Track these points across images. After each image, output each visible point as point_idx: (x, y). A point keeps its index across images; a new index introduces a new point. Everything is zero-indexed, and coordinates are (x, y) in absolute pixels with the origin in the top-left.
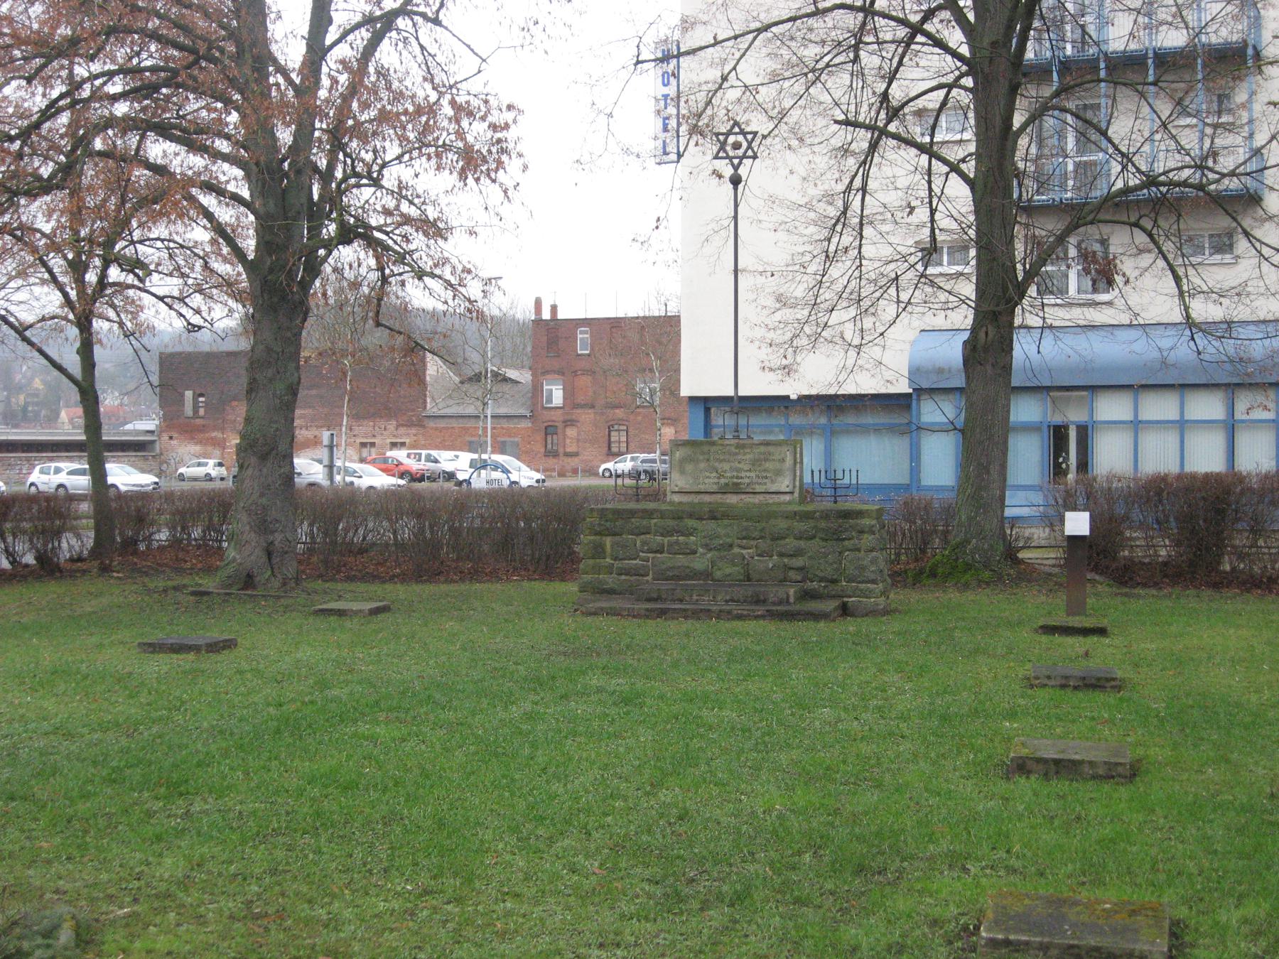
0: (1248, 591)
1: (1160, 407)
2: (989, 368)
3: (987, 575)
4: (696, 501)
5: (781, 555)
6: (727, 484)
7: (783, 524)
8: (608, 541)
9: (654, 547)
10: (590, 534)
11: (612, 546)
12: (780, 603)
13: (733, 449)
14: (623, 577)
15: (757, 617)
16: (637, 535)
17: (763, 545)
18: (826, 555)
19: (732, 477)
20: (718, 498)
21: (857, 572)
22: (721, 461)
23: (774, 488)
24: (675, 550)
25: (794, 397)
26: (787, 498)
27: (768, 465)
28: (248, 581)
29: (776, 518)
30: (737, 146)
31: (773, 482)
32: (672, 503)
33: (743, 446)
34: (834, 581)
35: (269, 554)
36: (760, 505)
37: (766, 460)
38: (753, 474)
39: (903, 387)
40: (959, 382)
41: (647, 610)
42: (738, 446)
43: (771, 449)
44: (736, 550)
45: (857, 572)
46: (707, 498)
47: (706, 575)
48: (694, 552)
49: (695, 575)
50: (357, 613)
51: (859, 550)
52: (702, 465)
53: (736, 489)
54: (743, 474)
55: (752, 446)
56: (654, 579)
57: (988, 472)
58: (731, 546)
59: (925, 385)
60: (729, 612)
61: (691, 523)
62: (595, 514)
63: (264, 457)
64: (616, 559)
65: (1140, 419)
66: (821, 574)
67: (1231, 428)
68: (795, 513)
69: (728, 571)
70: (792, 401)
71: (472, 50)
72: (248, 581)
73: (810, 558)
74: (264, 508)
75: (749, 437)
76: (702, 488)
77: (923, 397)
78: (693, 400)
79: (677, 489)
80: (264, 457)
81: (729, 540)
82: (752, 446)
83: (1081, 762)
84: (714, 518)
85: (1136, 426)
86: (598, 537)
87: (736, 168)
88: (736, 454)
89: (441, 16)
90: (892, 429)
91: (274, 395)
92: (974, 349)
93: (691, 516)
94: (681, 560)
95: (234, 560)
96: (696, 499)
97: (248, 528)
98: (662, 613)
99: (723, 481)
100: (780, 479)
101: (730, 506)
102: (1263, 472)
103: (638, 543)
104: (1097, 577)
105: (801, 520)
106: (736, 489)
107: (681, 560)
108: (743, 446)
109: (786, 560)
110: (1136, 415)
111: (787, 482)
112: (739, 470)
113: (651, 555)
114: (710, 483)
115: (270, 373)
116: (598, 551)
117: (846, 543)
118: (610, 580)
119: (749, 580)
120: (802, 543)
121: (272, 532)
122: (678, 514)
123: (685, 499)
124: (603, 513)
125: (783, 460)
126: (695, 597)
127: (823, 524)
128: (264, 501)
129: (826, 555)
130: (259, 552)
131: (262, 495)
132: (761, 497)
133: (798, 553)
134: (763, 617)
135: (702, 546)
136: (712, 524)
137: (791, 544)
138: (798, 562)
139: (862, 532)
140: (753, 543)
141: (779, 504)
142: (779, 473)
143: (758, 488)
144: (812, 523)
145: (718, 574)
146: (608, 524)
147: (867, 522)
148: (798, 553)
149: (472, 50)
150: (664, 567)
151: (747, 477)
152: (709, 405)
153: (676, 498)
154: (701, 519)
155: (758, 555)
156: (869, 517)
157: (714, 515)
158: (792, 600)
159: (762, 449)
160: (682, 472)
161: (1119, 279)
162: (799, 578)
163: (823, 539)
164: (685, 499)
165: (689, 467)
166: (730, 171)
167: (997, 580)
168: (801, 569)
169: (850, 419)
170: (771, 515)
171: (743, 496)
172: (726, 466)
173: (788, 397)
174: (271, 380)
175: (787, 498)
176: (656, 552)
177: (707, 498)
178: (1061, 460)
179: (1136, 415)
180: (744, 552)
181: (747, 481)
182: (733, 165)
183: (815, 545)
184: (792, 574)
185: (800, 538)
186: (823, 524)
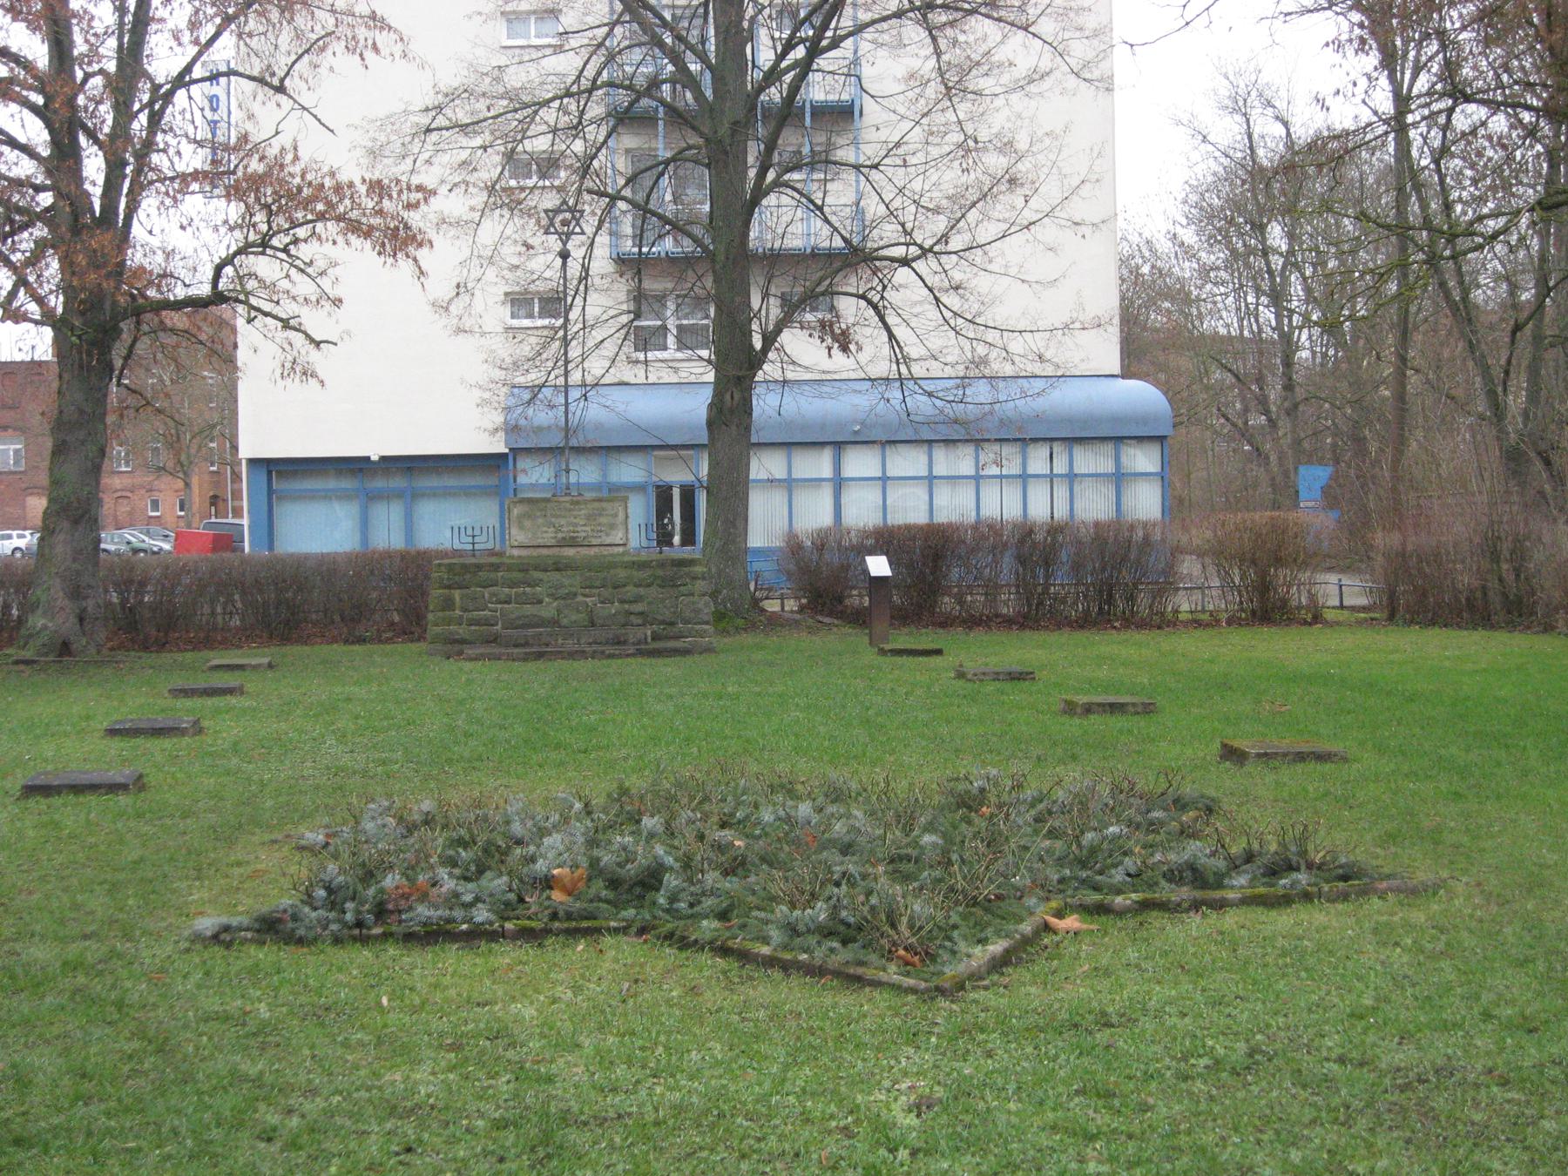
0: (970, 628)
1: (908, 462)
2: (734, 428)
3: (740, 622)
4: (535, 554)
5: (622, 602)
6: (564, 538)
7: (622, 574)
8: (457, 594)
9: (502, 597)
10: (440, 588)
11: (461, 599)
12: (639, 643)
13: (568, 505)
14: (473, 628)
15: (628, 656)
16: (484, 587)
17: (606, 593)
18: (663, 600)
19: (569, 531)
20: (555, 551)
21: (693, 615)
22: (560, 516)
23: (608, 541)
24: (522, 600)
25: (375, 458)
26: (621, 549)
27: (603, 520)
28: (65, 649)
29: (616, 567)
30: (565, 223)
31: (607, 535)
32: (512, 557)
33: (578, 503)
34: (672, 624)
35: (81, 620)
36: (596, 556)
37: (600, 515)
38: (588, 529)
39: (498, 446)
40: (704, 439)
41: (526, 653)
42: (572, 503)
43: (604, 505)
44: (580, 598)
45: (693, 615)
46: (545, 552)
47: (554, 622)
48: (540, 602)
49: (542, 623)
50: (255, 667)
51: (693, 595)
52: (540, 521)
53: (572, 542)
54: (579, 529)
55: (586, 502)
56: (503, 628)
57: (734, 526)
58: (575, 595)
59: (522, 444)
60: (603, 652)
61: (537, 575)
62: (443, 568)
63: (76, 522)
64: (465, 610)
65: (1076, 471)
66: (660, 618)
67: (839, 483)
68: (634, 563)
69: (574, 618)
70: (374, 462)
71: (319, 120)
72: (65, 649)
73: (649, 603)
74: (78, 573)
75: (580, 495)
76: (540, 542)
77: (793, 455)
78: (253, 462)
79: (516, 544)
80: (76, 522)
81: (574, 589)
82: (586, 502)
83: (1127, 704)
84: (558, 570)
85: (789, 485)
86: (447, 591)
87: (564, 244)
88: (570, 510)
89: (287, 82)
90: (485, 492)
91: (86, 457)
92: (720, 411)
93: (536, 568)
94: (529, 609)
95: (45, 627)
96: (535, 552)
97: (61, 594)
98: (540, 656)
99: (560, 535)
100: (614, 532)
101: (567, 557)
102: (871, 525)
103: (487, 595)
104: (836, 622)
105: (638, 570)
106: (572, 542)
107: (529, 609)
108: (578, 503)
109: (626, 606)
110: (1052, 469)
111: (620, 535)
112: (576, 525)
113: (499, 606)
114: (548, 536)
115: (81, 435)
116: (448, 604)
117: (682, 588)
118: (462, 631)
119: (593, 624)
120: (642, 591)
121: (85, 598)
122: (524, 567)
123: (524, 553)
124: (450, 567)
125: (616, 515)
126: (560, 641)
127: (660, 572)
128: (76, 566)
129: (663, 600)
130: (73, 620)
131: (74, 560)
132: (596, 550)
133: (637, 599)
134: (633, 655)
135: (548, 595)
136: (556, 576)
137: (631, 591)
138: (638, 607)
139: (695, 578)
140: (594, 591)
141: (612, 555)
142: (612, 526)
143: (594, 542)
144: (649, 572)
145: (565, 622)
146: (457, 578)
147: (699, 569)
148: (637, 599)
149: (319, 120)
150: (514, 616)
151: (583, 532)
152: (271, 468)
153: (516, 552)
154: (546, 570)
155: (602, 602)
156: (700, 564)
157: (559, 566)
158: (649, 640)
159: (596, 505)
160: (521, 527)
161: (852, 347)
162: (640, 621)
163: (660, 586)
164: (524, 553)
165: (527, 523)
166: (558, 246)
167: (751, 627)
168: (641, 614)
169: (431, 482)
170: (613, 565)
171: (579, 549)
172: (563, 522)
173: (369, 458)
174: (83, 443)
175: (621, 549)
176: (506, 602)
177: (545, 552)
178: (666, 521)
179: (1052, 469)
180: (588, 599)
181: (584, 534)
182: (561, 239)
183: (653, 591)
184: (633, 618)
185: (640, 586)
186: (660, 572)
